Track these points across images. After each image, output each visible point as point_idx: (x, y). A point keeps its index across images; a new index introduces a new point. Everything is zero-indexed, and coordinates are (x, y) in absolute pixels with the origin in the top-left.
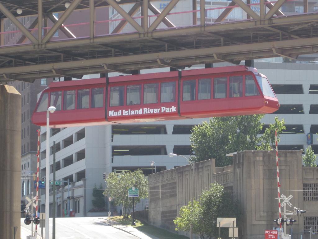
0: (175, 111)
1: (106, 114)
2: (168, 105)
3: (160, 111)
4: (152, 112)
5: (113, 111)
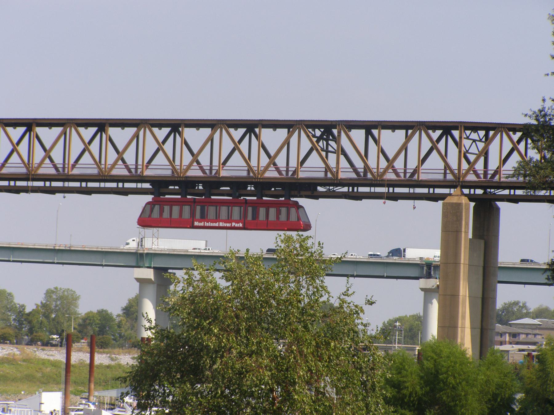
0: (195, 225)
1: (193, 223)
2: (237, 222)
3: (231, 225)
4: (225, 226)
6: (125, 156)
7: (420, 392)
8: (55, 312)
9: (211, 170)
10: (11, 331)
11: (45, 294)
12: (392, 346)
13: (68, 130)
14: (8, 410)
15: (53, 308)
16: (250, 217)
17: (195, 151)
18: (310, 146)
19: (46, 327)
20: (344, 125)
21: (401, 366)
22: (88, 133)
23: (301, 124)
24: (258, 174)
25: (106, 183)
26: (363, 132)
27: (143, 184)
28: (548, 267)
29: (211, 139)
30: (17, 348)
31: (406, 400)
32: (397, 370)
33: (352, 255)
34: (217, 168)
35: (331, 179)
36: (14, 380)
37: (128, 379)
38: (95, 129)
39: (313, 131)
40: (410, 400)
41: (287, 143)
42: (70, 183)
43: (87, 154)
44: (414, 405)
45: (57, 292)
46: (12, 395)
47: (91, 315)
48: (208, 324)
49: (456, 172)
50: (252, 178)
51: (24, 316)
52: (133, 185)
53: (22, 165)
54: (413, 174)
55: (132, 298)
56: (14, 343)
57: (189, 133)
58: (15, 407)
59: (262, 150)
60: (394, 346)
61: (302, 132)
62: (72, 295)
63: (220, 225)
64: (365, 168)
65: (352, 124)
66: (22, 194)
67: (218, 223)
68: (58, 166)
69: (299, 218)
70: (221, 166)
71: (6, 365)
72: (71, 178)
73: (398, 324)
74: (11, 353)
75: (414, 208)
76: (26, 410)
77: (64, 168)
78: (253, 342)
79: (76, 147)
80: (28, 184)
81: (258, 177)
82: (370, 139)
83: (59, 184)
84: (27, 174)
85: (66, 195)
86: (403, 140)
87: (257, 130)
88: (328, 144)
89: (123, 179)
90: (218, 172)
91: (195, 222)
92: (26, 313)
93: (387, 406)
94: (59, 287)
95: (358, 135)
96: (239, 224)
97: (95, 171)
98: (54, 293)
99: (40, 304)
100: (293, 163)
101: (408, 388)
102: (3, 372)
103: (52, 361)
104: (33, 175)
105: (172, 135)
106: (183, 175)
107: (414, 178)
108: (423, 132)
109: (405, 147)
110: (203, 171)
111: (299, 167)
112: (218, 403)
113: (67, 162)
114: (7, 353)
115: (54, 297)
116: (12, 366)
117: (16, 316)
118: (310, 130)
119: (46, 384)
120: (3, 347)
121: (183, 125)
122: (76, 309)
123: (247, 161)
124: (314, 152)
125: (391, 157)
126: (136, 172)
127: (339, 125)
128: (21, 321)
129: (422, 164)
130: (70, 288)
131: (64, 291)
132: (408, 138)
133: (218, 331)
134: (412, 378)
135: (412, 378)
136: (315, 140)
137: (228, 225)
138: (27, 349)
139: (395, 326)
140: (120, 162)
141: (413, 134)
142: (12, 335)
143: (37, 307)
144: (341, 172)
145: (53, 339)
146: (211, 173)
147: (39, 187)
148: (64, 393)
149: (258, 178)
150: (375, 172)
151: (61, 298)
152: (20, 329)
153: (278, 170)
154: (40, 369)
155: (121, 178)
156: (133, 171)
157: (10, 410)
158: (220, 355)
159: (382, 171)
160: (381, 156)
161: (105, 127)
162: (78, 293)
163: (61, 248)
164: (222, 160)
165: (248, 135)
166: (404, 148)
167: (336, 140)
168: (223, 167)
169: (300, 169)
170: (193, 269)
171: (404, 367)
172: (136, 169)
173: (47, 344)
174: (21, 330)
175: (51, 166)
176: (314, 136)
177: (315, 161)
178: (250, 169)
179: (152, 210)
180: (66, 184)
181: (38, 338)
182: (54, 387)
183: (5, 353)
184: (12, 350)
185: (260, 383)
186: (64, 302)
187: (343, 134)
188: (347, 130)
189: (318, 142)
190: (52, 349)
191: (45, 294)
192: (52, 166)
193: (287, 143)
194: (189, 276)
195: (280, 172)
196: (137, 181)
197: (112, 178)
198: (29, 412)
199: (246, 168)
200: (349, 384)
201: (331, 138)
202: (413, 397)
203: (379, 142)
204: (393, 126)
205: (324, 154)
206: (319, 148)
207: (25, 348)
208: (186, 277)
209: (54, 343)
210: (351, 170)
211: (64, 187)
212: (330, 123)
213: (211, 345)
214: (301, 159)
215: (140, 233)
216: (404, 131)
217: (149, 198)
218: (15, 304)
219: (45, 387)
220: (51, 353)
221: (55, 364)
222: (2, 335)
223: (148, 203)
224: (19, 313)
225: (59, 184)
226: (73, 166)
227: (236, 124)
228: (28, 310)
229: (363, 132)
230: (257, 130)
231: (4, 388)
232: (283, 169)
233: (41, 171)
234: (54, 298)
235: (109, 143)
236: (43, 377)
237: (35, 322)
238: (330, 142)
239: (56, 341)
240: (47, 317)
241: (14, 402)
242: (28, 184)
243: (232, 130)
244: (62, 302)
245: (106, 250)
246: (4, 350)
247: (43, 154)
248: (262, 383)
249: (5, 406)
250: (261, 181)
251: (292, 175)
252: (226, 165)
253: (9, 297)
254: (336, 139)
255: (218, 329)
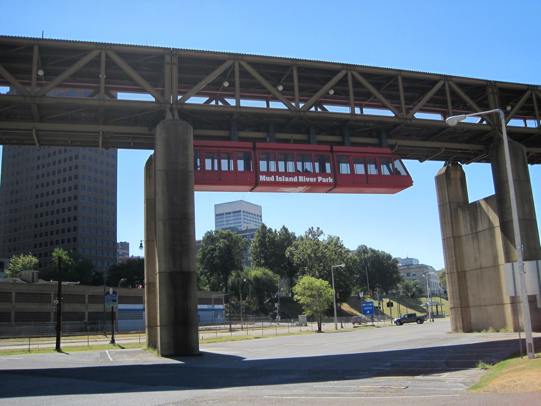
3: (317, 180)
4: (308, 181)
28: (13, 282)
55: (382, 251)
63: (300, 181)
67: (296, 177)
91: (261, 176)
94: (383, 251)
96: (327, 179)
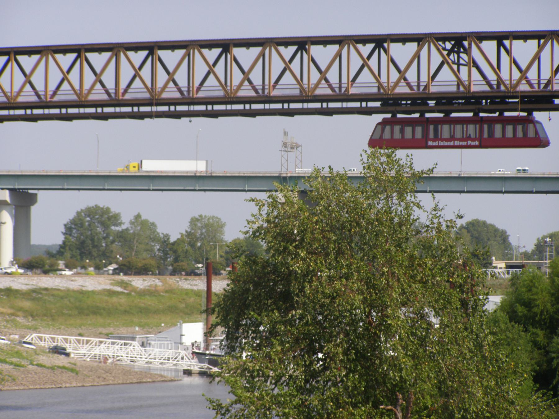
0: (429, 144)
1: (427, 143)
2: (473, 140)
3: (467, 143)
4: (461, 144)
5: (431, 142)
6: (328, 76)
7: (552, 310)
8: (200, 240)
9: (340, 88)
10: (153, 262)
11: (189, 222)
12: (543, 263)
13: (191, 51)
14: (147, 343)
15: (199, 236)
16: (486, 135)
17: (246, 68)
18: (440, 59)
19: (191, 255)
20: (434, 37)
21: (531, 284)
22: (212, 54)
23: (431, 37)
24: (389, 89)
25: (309, 104)
26: (494, 43)
27: (309, 104)
29: (339, 55)
30: (159, 279)
31: (537, 319)
32: (527, 288)
33: (500, 171)
34: (346, 85)
35: (463, 93)
36: (157, 312)
37: (217, 309)
38: (220, 50)
39: (443, 43)
40: (541, 318)
41: (417, 56)
42: (349, 103)
43: (211, 76)
44: (545, 324)
45: (202, 220)
46: (155, 328)
47: (238, 242)
48: (295, 247)
49: (78, 92)
50: (382, 94)
51: (169, 245)
52: (338, 105)
53: (145, 90)
54: (547, 85)
56: (156, 273)
57: (316, 50)
58: (155, 340)
59: (391, 65)
60: (545, 263)
61: (432, 46)
62: (218, 222)
64: (498, 80)
65: (483, 35)
66: (147, 120)
68: (183, 89)
69: (536, 132)
70: (350, 83)
71: (147, 297)
72: (196, 101)
73: (548, 240)
74: (153, 284)
75: (550, 120)
76: (166, 342)
77: (189, 91)
78: (343, 265)
79: (201, 69)
80: (152, 109)
81: (388, 93)
82: (502, 50)
83: (184, 108)
84: (150, 99)
85: (192, 119)
86: (536, 49)
87: (386, 45)
88: (459, 57)
89: (102, 104)
90: (347, 90)
92: (171, 242)
93: (517, 325)
94: (203, 215)
95: (490, 46)
97: (221, 93)
98: (199, 221)
99: (184, 233)
100: (424, 78)
101: (539, 305)
102: (144, 304)
103: (195, 290)
104: (157, 100)
105: (377, 51)
106: (311, 94)
107: (549, 88)
108: (351, 46)
109: (538, 57)
110: (332, 89)
111: (431, 82)
112: (309, 330)
113: (191, 85)
114: (149, 284)
115: (199, 225)
116: (154, 298)
117: (161, 246)
118: (440, 43)
119: (189, 314)
120: (145, 278)
121: (309, 43)
122: (222, 236)
123: (377, 78)
124: (446, 66)
125: (524, 67)
126: (264, 92)
127: (469, 36)
128: (166, 250)
129: (556, 74)
130: (216, 216)
131: (209, 219)
132: (541, 48)
133: (305, 254)
134: (543, 296)
135: (543, 296)
136: (445, 53)
137: (464, 143)
138: (169, 279)
139: (546, 242)
140: (246, 83)
141: (545, 44)
142: (153, 266)
143: (182, 236)
144: (474, 85)
145: (198, 268)
146: (340, 90)
147: (239, 110)
148: (205, 324)
149: (388, 94)
150: (508, 84)
151: (207, 226)
152: (165, 259)
153: (409, 85)
154: (184, 299)
155: (248, 100)
156: (260, 91)
157: (150, 344)
158: (308, 279)
159: (515, 82)
160: (514, 67)
161: (229, 47)
162: (223, 220)
163: (202, 175)
164: (351, 78)
165: (377, 50)
166: (537, 57)
167: (467, 51)
168: (352, 84)
169: (432, 83)
170: (276, 191)
171: (534, 284)
172: (263, 89)
173: (193, 273)
174: (166, 260)
175: (176, 89)
176: (444, 49)
177: (446, 74)
178: (380, 86)
179: (383, 130)
180: (192, 108)
181: (181, 267)
182: (198, 317)
183: (147, 284)
184: (154, 281)
185: (351, 307)
186: (210, 230)
187: (474, 46)
188: (478, 42)
189: (449, 55)
190: (195, 279)
191: (189, 222)
192: (327, 86)
193: (417, 56)
194: (273, 199)
195: (411, 87)
196: (342, 101)
197: (238, 100)
198: (170, 345)
199: (377, 85)
200: (447, 305)
201: (462, 50)
202: (544, 315)
203: (511, 53)
204: (525, 36)
205: (455, 67)
206: (450, 61)
207: (168, 279)
208: (270, 200)
209: (199, 272)
210: (484, 83)
211: (189, 111)
212: (460, 35)
213: (298, 270)
214: (432, 74)
215: (282, 156)
216: (536, 41)
217: (378, 118)
218: (158, 234)
219: (188, 318)
220: (194, 282)
221: (197, 294)
222: (144, 266)
223: (379, 124)
224: (163, 243)
225: (184, 108)
226: (199, 89)
227: (364, 40)
228: (172, 240)
229: (494, 43)
230: (386, 45)
231: (146, 321)
232: (414, 84)
233: (165, 95)
234: (199, 226)
235: (234, 63)
236: (186, 307)
237: (180, 251)
238: (461, 55)
239: (201, 270)
240: (192, 245)
241: (153, 335)
242: (152, 109)
243: (360, 46)
244: (207, 230)
245: (248, 175)
246: (146, 282)
247: (166, 77)
248: (354, 308)
249: (145, 340)
250: (468, 95)
251: (424, 90)
252: (279, 83)
253: (152, 227)
254: (467, 51)
255: (305, 253)
